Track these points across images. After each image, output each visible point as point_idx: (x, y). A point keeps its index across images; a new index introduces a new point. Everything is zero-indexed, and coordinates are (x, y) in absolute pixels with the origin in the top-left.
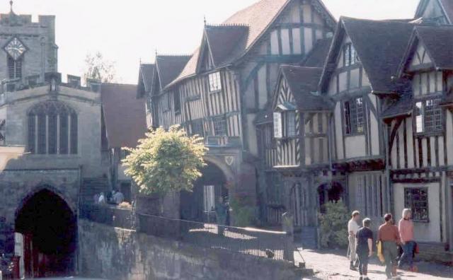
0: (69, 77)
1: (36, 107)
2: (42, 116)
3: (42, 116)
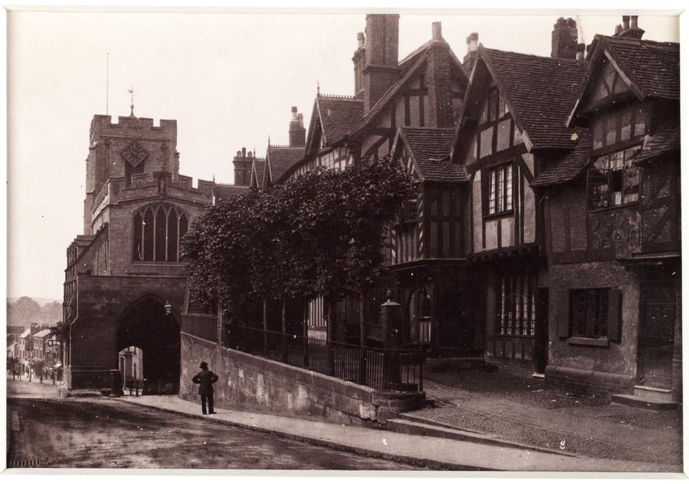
0: (200, 182)
1: (142, 209)
2: (149, 219)
3: (149, 219)
